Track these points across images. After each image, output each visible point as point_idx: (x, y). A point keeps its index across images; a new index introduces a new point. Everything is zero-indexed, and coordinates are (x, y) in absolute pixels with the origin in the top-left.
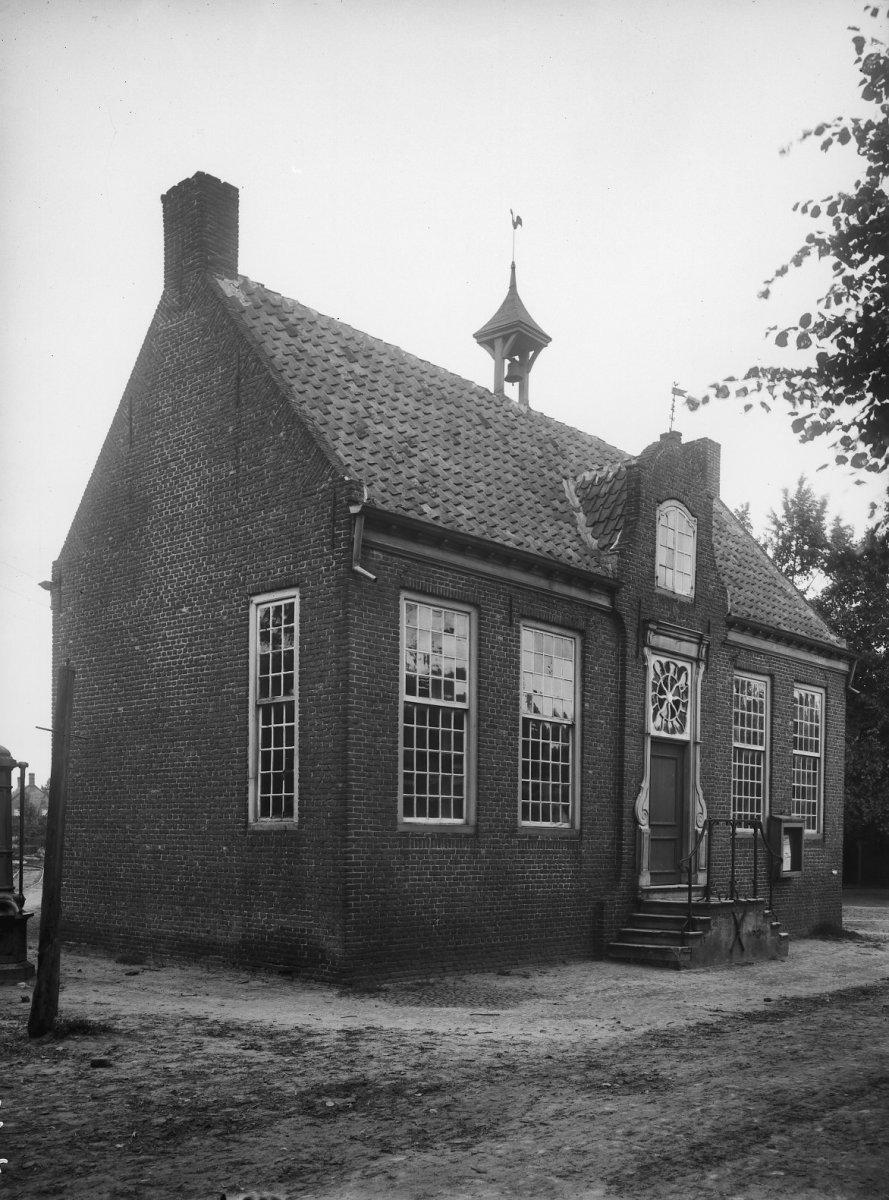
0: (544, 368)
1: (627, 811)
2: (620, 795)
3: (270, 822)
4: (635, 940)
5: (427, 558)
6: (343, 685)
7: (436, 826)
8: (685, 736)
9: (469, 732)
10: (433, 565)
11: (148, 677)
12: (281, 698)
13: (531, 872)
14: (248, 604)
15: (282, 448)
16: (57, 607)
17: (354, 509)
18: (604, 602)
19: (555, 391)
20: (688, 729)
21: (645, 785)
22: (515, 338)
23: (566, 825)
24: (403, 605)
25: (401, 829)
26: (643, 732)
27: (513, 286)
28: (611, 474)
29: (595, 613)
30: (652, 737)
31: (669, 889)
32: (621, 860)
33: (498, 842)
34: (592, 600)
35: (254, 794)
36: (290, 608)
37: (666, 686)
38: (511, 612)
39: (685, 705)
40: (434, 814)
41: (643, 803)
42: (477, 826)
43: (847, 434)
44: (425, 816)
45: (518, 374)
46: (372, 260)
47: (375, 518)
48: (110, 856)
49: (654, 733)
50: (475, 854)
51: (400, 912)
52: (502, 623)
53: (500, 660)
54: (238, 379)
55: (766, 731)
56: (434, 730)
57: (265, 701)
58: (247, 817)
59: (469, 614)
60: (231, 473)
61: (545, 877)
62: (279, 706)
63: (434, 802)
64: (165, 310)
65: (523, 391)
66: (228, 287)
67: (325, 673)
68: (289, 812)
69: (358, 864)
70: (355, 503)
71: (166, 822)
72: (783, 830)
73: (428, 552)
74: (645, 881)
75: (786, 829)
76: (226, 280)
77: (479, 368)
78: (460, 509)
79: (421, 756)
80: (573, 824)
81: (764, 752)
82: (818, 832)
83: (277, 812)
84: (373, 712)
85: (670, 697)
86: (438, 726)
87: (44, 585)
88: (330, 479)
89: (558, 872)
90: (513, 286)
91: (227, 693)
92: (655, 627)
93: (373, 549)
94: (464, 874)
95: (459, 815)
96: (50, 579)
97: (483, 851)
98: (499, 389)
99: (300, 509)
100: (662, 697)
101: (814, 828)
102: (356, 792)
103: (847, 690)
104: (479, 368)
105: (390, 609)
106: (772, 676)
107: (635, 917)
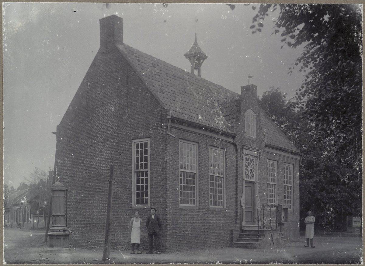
0: (205, 65)
1: (239, 202)
2: (236, 198)
3: (140, 206)
4: (242, 241)
6: (165, 166)
9: (196, 179)
11: (95, 163)
12: (144, 170)
14: (132, 142)
15: (143, 98)
16: (58, 140)
17: (168, 117)
18: (231, 140)
19: (209, 73)
20: (254, 178)
21: (244, 194)
22: (197, 57)
23: (222, 207)
24: (180, 143)
25: (180, 207)
26: (243, 179)
28: (230, 100)
29: (229, 143)
30: (245, 181)
32: (237, 217)
35: (134, 198)
36: (146, 144)
37: (248, 165)
38: (207, 144)
39: (254, 171)
40: (188, 203)
41: (243, 200)
42: (199, 207)
43: (301, 88)
44: (185, 204)
45: (197, 67)
46: (158, 35)
47: (173, 120)
48: (81, 217)
49: (245, 179)
53: (204, 158)
54: (128, 77)
55: (276, 178)
57: (137, 171)
58: (132, 205)
59: (196, 145)
60: (125, 103)
62: (142, 172)
64: (100, 53)
65: (199, 73)
66: (121, 47)
67: (159, 163)
68: (147, 202)
70: (169, 115)
71: (102, 207)
72: (282, 209)
74: (244, 224)
75: (283, 208)
76: (120, 45)
77: (186, 66)
78: (192, 114)
79: (142, 183)
80: (224, 207)
81: (223, 177)
82: (292, 210)
83: (142, 203)
85: (250, 168)
87: (54, 133)
88: (160, 108)
89: (220, 221)
91: (124, 168)
95: (194, 203)
96: (55, 131)
98: (192, 72)
99: (149, 115)
100: (247, 168)
101: (291, 208)
102: (169, 197)
103: (299, 165)
104: (186, 66)
105: (177, 145)
106: (278, 161)
107: (241, 235)
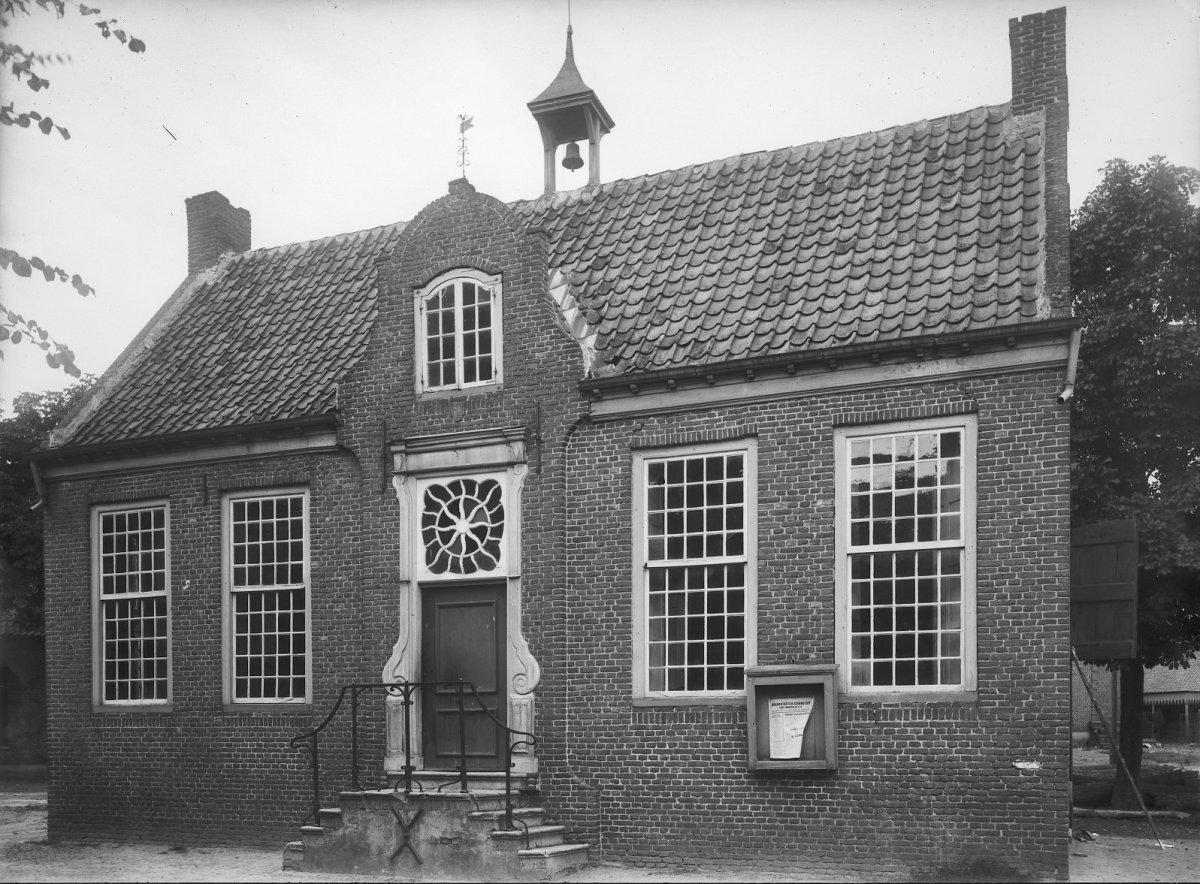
5: (107, 472)
7: (150, 706)
8: (501, 570)
10: (117, 476)
13: (239, 750)
18: (328, 442)
22: (570, 117)
27: (570, 53)
31: (444, 776)
33: (197, 720)
34: (311, 445)
50: (171, 732)
51: (94, 782)
52: (195, 505)
56: (285, 635)
61: (258, 756)
63: (123, 686)
69: (56, 740)
73: (108, 467)
84: (66, 615)
86: (683, 670)
90: (570, 53)
92: (403, 448)
93: (62, 482)
94: (159, 750)
95: (162, 694)
97: (179, 729)
